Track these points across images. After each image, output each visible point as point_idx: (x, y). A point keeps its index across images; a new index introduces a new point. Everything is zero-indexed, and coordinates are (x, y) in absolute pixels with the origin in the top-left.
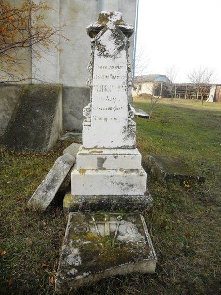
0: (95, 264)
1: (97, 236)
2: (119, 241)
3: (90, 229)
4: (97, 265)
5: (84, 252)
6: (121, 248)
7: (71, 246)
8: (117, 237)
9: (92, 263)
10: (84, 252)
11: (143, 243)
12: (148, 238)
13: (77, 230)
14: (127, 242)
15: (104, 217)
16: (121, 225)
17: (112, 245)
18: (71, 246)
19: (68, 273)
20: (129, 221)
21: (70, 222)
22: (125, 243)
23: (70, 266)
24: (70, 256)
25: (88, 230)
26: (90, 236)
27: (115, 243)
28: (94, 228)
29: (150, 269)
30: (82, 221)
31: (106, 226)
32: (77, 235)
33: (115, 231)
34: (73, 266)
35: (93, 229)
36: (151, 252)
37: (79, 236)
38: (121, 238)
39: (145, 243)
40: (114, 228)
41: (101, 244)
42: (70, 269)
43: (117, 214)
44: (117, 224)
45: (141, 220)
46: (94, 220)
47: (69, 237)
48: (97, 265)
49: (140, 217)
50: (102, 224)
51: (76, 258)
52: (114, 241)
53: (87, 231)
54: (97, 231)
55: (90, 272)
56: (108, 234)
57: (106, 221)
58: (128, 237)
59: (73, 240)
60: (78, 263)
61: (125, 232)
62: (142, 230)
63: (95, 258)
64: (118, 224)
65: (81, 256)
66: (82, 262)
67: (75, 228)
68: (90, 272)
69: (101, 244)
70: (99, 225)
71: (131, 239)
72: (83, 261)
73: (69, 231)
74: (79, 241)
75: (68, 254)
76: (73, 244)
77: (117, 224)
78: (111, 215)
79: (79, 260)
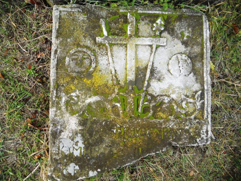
0: (107, 152)
1: (110, 82)
2: (153, 96)
3: (97, 62)
4: (111, 154)
5: (88, 126)
6: (154, 116)
7: (30, 159)
8: (149, 85)
9: (102, 150)
10: (88, 126)
11: (194, 103)
12: (207, 90)
13: (72, 64)
14: (166, 100)
15: (126, 21)
16: (160, 49)
17: (138, 106)
18: (63, 108)
19: (65, 172)
20: (177, 37)
21: (57, 37)
22: (162, 103)
23: (66, 156)
24: (65, 135)
25: (93, 65)
26: (98, 80)
27: (143, 103)
28: (105, 58)
29: (88, 103)
30: (82, 37)
31: (131, 51)
32: (73, 79)
33: (146, 68)
34: (70, 158)
35: (103, 61)
36: (204, 128)
37: (76, 82)
38: (156, 88)
39: (198, 104)
40: (144, 55)
41: (119, 105)
42: (66, 165)
43: (7, 156)
44: (151, 46)
45: (202, 35)
46: (105, 33)
47: (58, 86)
48: (111, 154)
49: (202, 24)
50: (121, 45)
51: (75, 140)
52: (143, 95)
53: (91, 69)
54: (111, 68)
55: (99, 170)
56: (131, 77)
57: (131, 36)
58: (171, 86)
59: (67, 93)
60: (79, 151)
61: (164, 71)
62: (198, 65)
63: (107, 140)
64: (154, 47)
65: (83, 136)
66: (86, 148)
67: (67, 59)
68: (99, 170)
69: (119, 105)
70: (115, 48)
71: (174, 92)
72: (88, 146)
73: (57, 65)
74: (78, 97)
75: (61, 131)
76: (67, 102)
77: (151, 46)
78: (141, 15)
79: (81, 144)
